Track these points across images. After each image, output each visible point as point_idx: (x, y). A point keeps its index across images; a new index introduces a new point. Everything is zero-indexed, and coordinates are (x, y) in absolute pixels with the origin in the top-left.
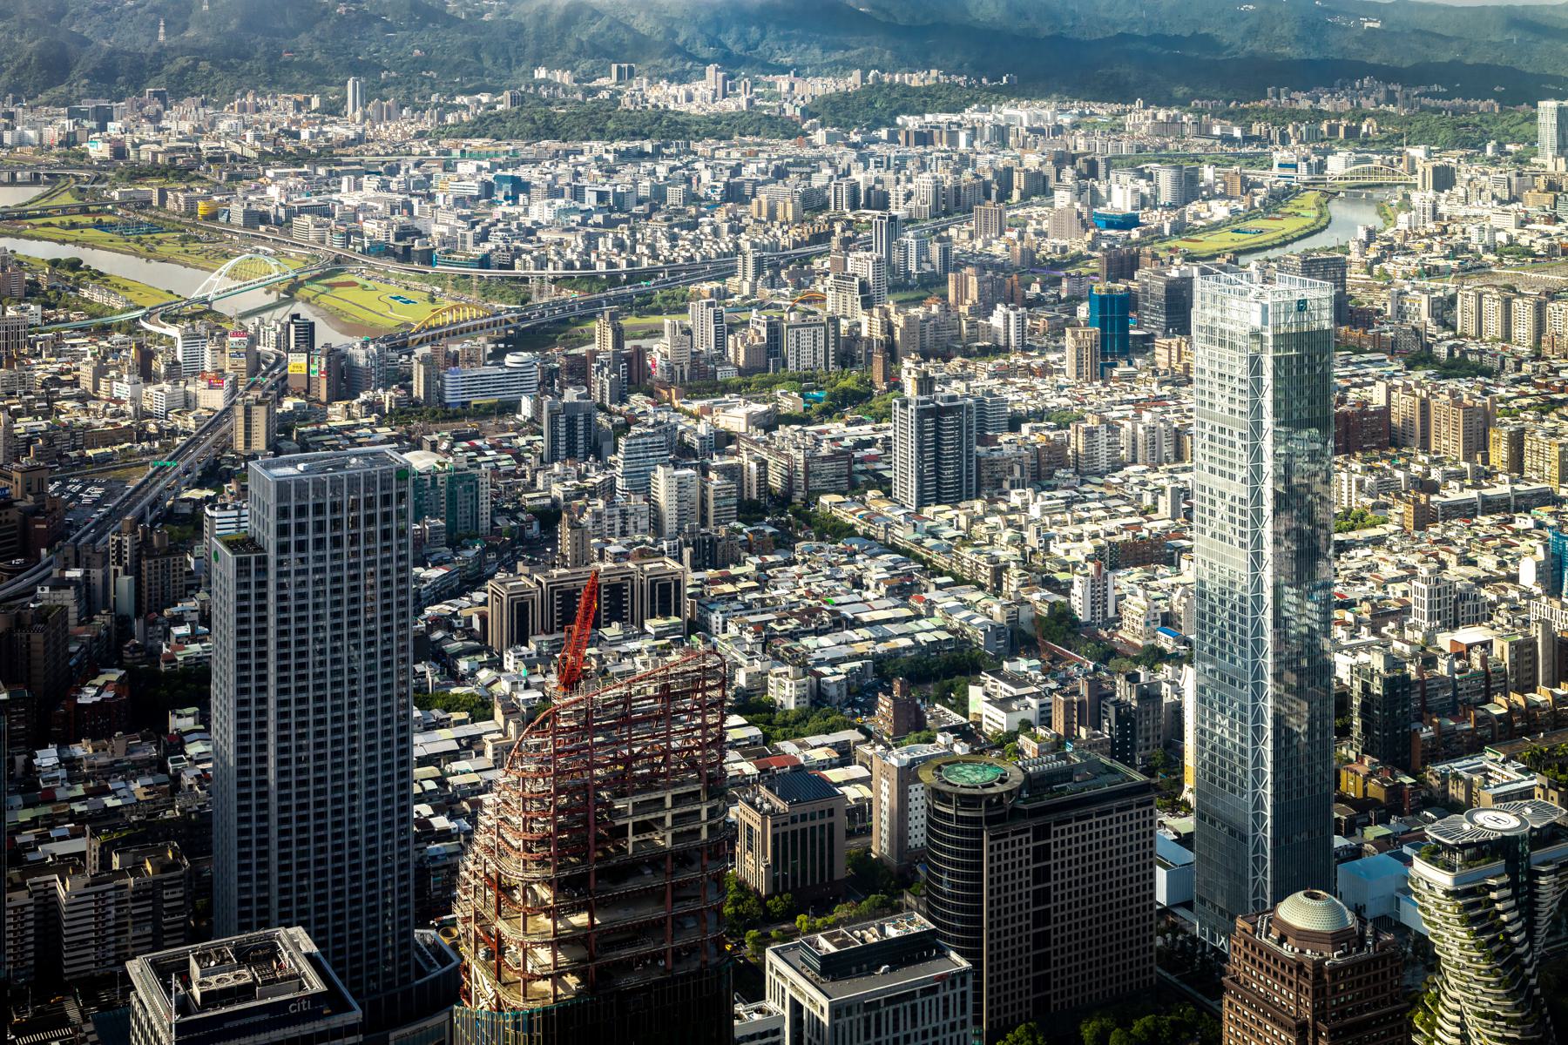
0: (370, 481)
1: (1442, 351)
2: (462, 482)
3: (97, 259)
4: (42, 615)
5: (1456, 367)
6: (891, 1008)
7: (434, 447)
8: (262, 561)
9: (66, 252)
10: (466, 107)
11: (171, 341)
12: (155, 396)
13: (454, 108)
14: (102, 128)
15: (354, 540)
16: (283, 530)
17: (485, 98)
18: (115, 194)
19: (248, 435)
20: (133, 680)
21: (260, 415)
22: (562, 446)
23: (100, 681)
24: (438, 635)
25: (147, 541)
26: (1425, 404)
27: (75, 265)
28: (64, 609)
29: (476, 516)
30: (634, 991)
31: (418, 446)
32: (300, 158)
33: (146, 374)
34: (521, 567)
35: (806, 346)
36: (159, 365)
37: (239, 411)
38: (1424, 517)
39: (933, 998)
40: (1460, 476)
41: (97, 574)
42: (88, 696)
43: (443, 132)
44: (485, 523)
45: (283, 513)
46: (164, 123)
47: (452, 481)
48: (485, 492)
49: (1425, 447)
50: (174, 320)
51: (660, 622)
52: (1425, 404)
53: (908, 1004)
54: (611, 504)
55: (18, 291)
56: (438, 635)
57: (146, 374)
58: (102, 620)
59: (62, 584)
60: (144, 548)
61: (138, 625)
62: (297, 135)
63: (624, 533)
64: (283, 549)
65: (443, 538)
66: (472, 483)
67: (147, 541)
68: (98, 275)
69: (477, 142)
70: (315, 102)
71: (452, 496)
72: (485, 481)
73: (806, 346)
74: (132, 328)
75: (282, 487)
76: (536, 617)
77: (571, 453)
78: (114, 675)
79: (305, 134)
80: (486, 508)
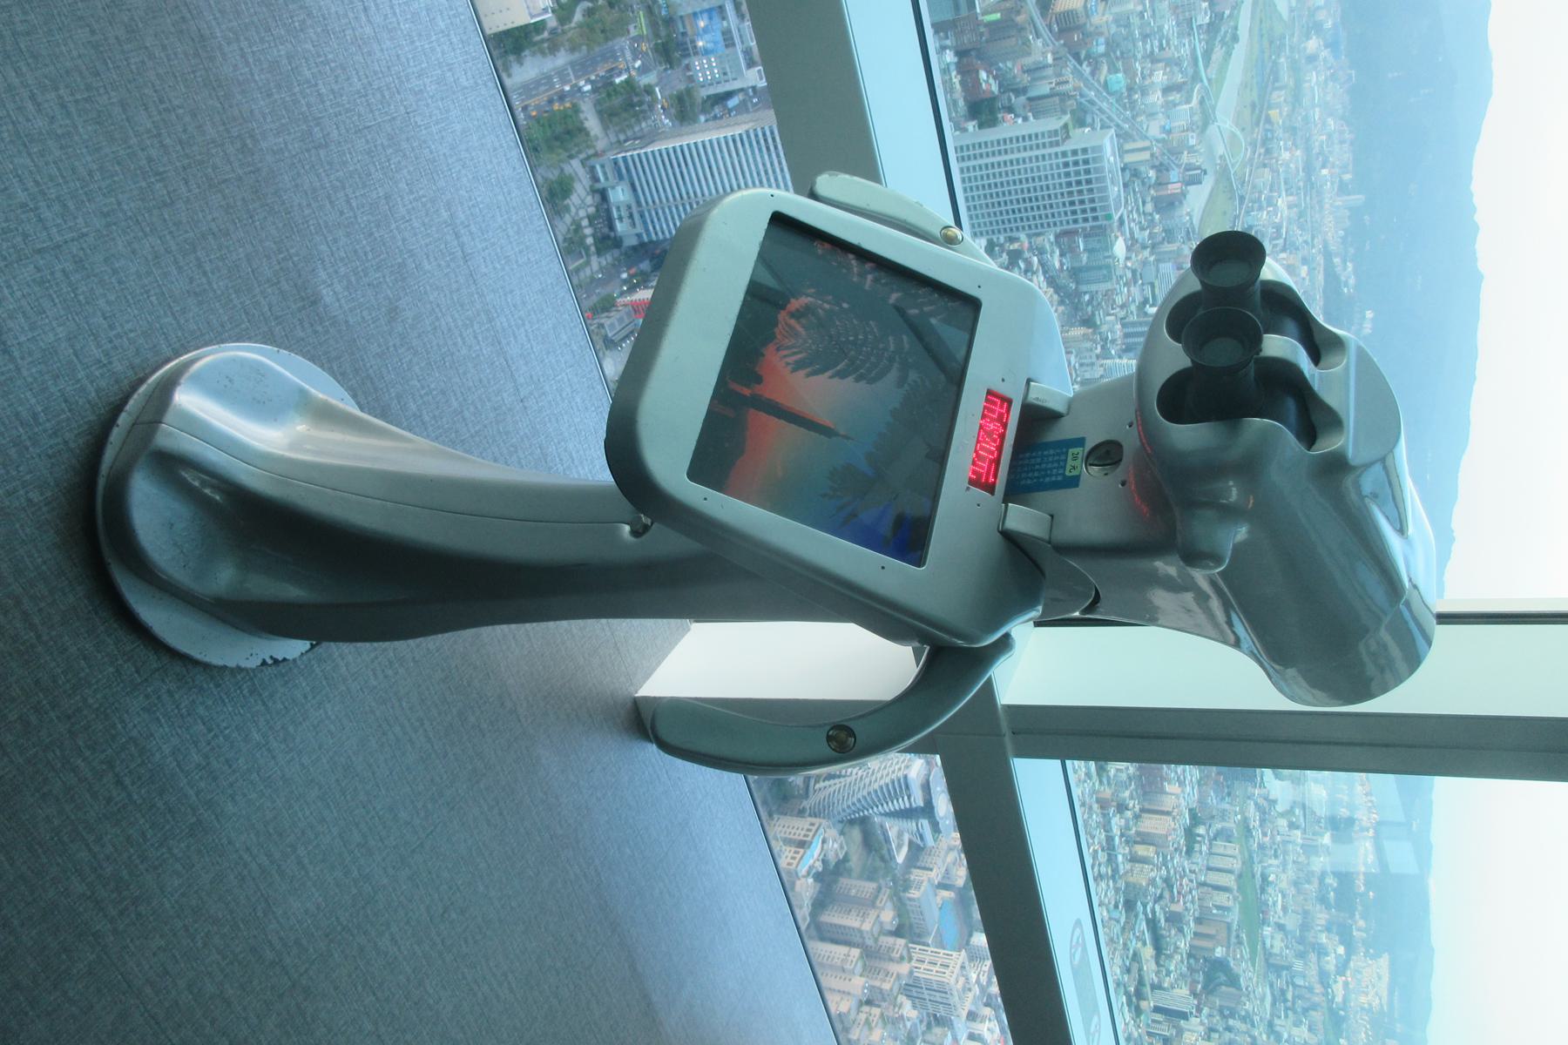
0: (1104, 199)
1: (1201, 830)
2: (1106, 270)
3: (1240, 51)
4: (1026, 43)
5: (1190, 834)
7: (1128, 258)
8: (1057, 144)
9: (1243, 32)
10: (1345, 269)
11: (1188, 101)
12: (1156, 98)
13: (1344, 262)
14: (1326, 46)
15: (1074, 213)
16: (1075, 152)
17: (1352, 281)
18: (1282, 60)
19: (1133, 151)
20: (992, 100)
21: (1146, 156)
22: (1131, 330)
23: (991, 81)
24: (1022, 265)
25: (1070, 97)
26: (1168, 813)
27: (1235, 39)
28: (1029, 54)
29: (1089, 282)
30: (978, 79)
31: (1129, 249)
32: (1308, 169)
33: (1167, 90)
34: (1061, 308)
36: (1175, 97)
37: (1147, 144)
38: (1103, 804)
40: (1128, 828)
41: (1050, 71)
42: (983, 75)
43: (1328, 255)
44: (1084, 288)
45: (1085, 151)
46: (1331, 84)
47: (1108, 267)
48: (1103, 287)
49: (1143, 810)
50: (1202, 102)
52: (1168, 813)
54: (1098, 357)
55: (1218, 9)
56: (1022, 265)
57: (1167, 90)
58: (1026, 78)
59: (1044, 54)
60: (1064, 96)
61: (1022, 99)
62: (1324, 167)
63: (1081, 365)
64: (1064, 154)
65: (1076, 265)
66: (1108, 278)
67: (1070, 97)
68: (1228, 54)
69: (1321, 277)
70: (1347, 177)
71: (1100, 268)
72: (1108, 286)
74: (1196, 78)
75: (1099, 149)
77: (1127, 335)
78: (995, 88)
79: (1325, 172)
80: (1093, 287)
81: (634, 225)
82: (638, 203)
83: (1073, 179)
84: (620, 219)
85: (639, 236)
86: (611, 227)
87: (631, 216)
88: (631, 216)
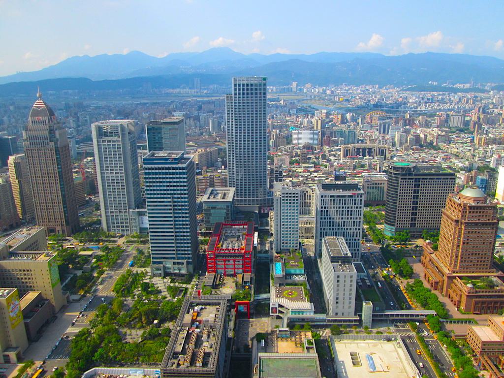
6: (338, 199)
16: (235, 90)
35: (456, 120)
39: (352, 199)
45: (235, 85)
51: (379, 156)
53: (344, 199)
73: (456, 120)
76: (350, 153)
81: (183, 264)
82: (174, 258)
83: (250, 92)
84: (179, 269)
85: (188, 263)
86: (183, 275)
87: (179, 263)
88: (179, 263)
